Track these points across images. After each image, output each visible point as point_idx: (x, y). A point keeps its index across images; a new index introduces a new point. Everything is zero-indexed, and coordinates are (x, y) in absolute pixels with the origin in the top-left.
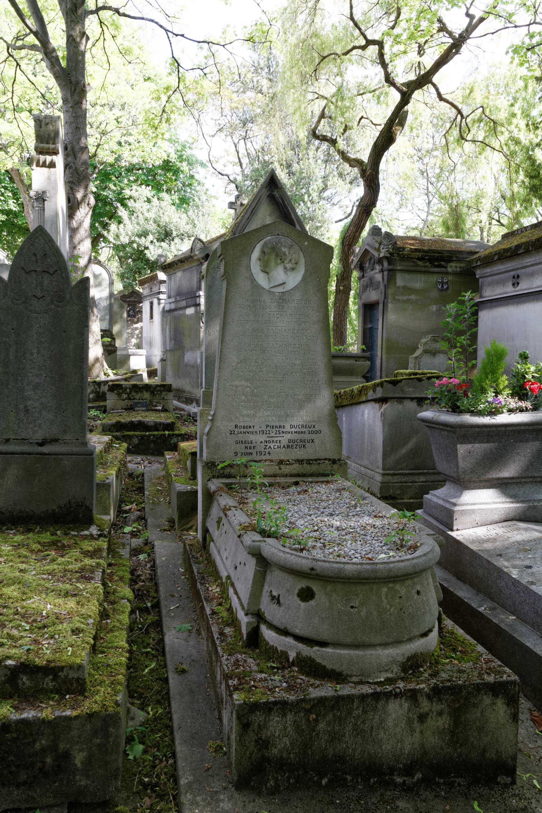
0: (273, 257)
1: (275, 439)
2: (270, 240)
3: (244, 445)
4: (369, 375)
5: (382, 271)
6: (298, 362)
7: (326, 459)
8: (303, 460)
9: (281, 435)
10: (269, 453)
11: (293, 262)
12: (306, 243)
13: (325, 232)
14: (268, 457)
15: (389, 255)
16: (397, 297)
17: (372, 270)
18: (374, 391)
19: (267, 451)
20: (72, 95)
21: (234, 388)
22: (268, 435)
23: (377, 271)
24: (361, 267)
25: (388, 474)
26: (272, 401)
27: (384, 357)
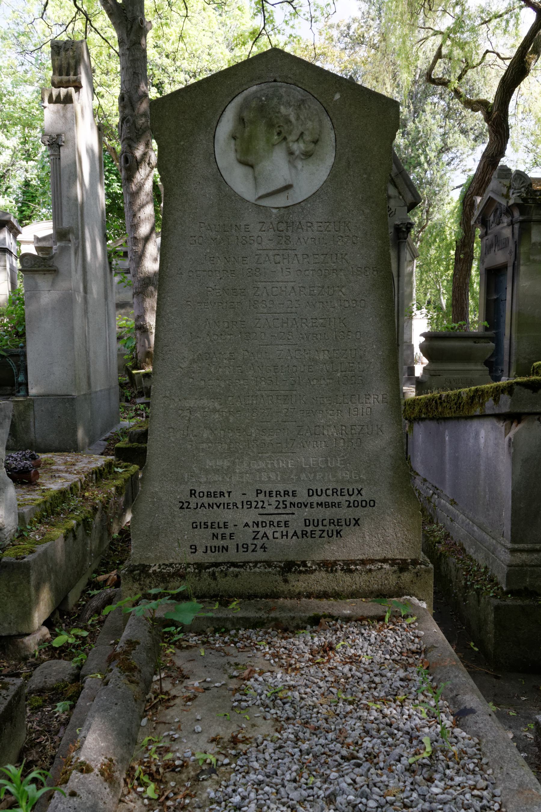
0: (261, 128)
1: (276, 519)
2: (256, 92)
3: (210, 531)
4: (493, 360)
5: (512, 224)
6: (322, 356)
7: (385, 561)
8: (335, 563)
9: (288, 511)
10: (263, 547)
11: (308, 137)
12: (337, 96)
13: (445, 196)
14: (260, 555)
15: (521, 202)
16: (532, 258)
17: (498, 224)
18: (496, 400)
19: (259, 543)
20: (128, 35)
21: (187, 413)
22: (261, 511)
23: (505, 224)
24: (484, 222)
25: (521, 551)
26: (268, 439)
27: (514, 336)
